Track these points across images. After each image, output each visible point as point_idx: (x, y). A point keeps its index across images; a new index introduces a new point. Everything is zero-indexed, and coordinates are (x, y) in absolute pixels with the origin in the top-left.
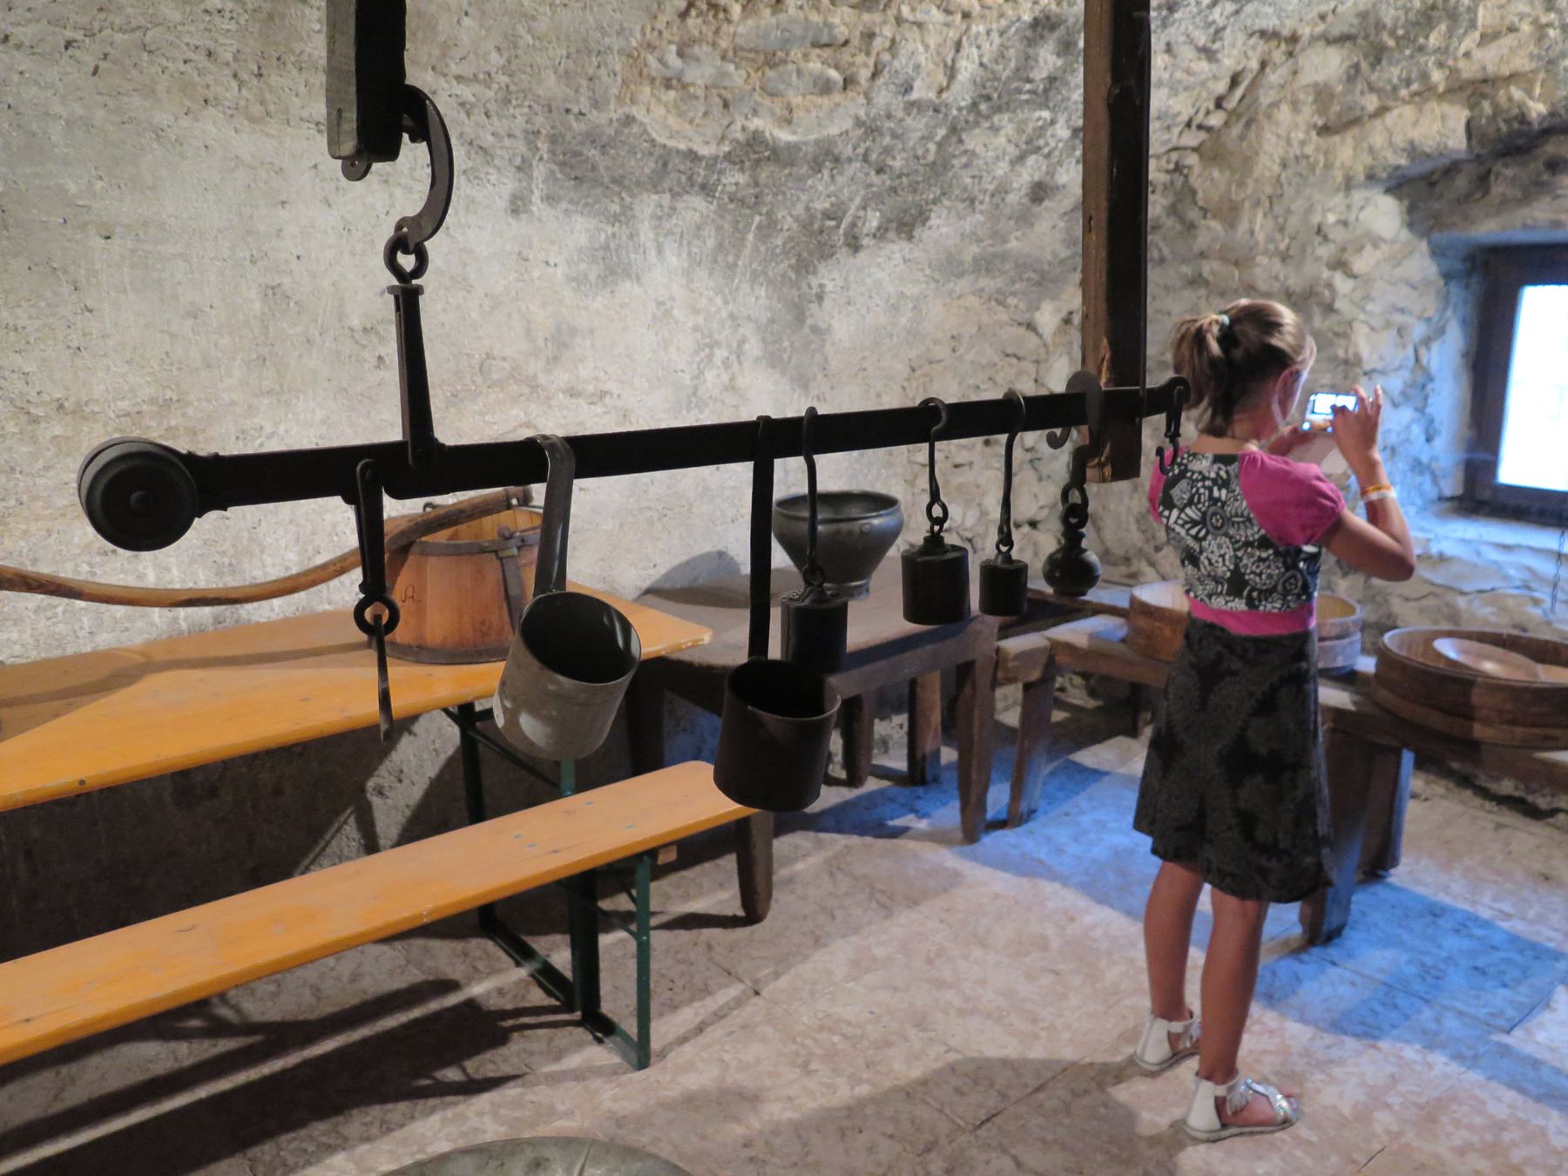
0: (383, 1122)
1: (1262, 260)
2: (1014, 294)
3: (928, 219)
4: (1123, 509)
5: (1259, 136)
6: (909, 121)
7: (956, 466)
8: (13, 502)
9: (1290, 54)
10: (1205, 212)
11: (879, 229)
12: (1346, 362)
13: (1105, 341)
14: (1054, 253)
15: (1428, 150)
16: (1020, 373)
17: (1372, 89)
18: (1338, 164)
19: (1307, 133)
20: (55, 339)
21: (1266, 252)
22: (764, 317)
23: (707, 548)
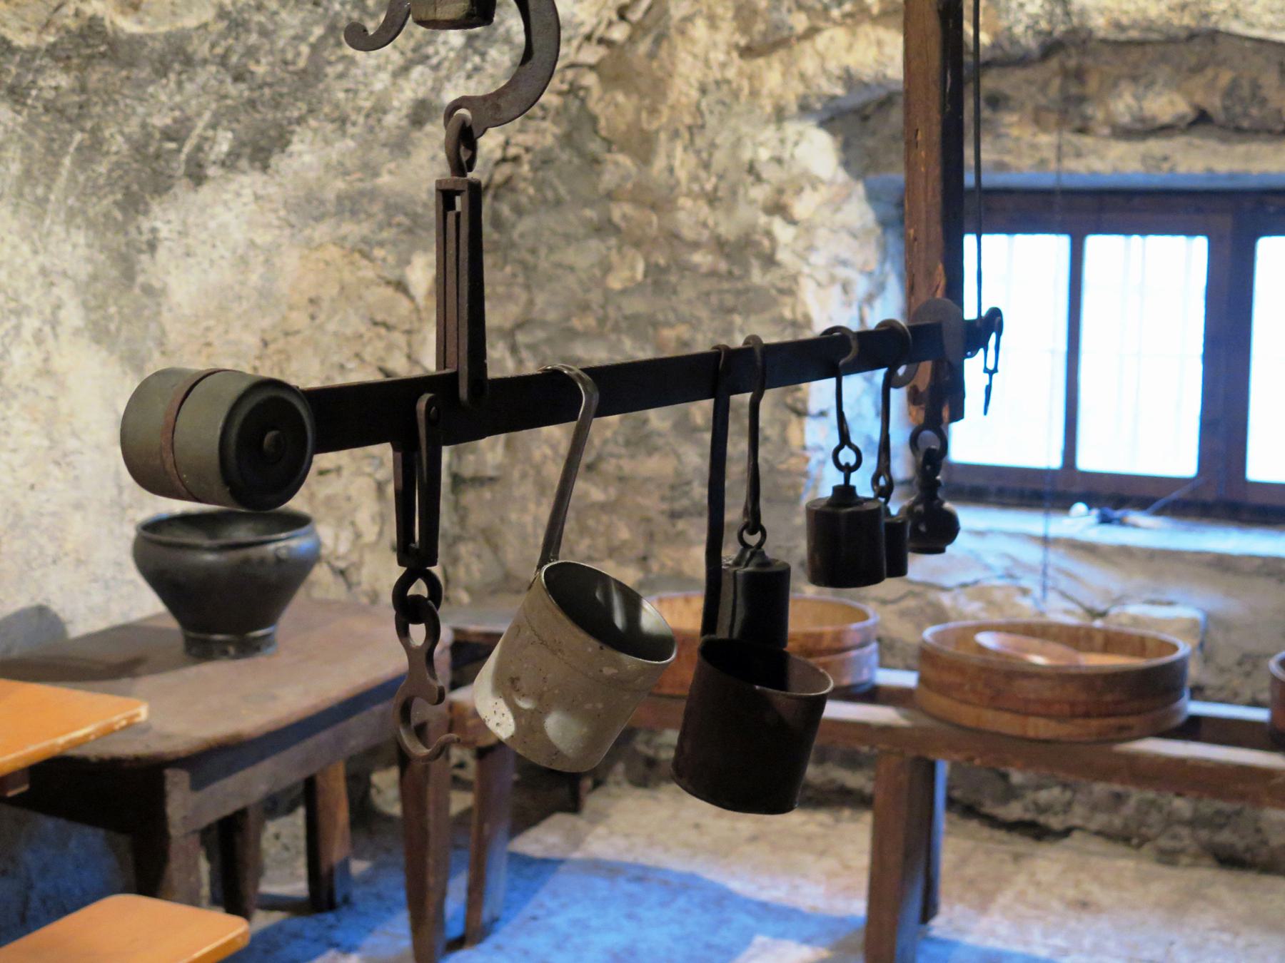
1: (685, 202)
2: (381, 244)
3: (288, 143)
4: (528, 519)
5: (672, 55)
6: (284, 15)
10: (609, 143)
11: (229, 154)
13: (940, 267)
15: (866, 79)
16: (390, 347)
18: (765, 91)
19: (728, 53)
21: (689, 194)
22: (84, 271)
23: (22, 601)
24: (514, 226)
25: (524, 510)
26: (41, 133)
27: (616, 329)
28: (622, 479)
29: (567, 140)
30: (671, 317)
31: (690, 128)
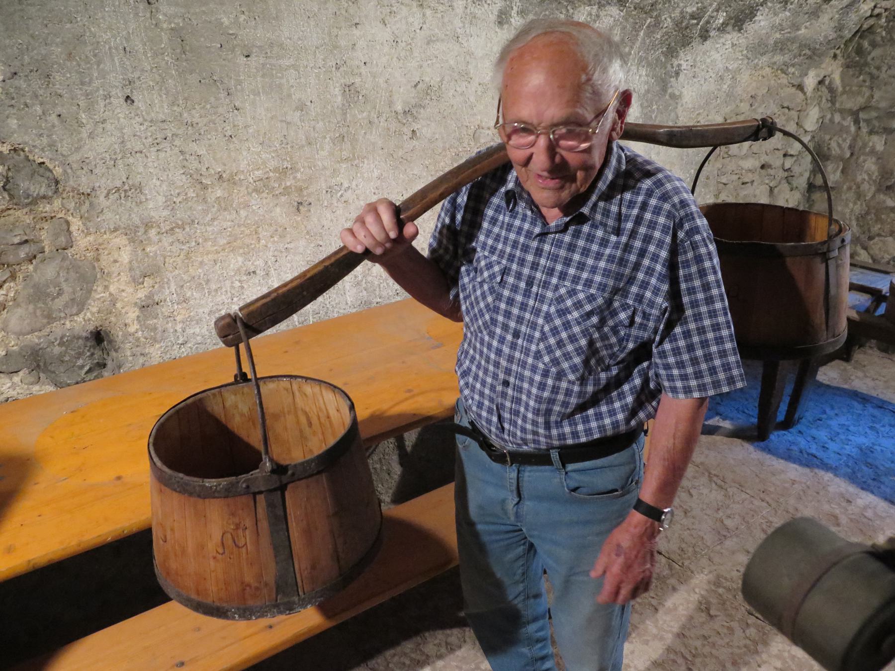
0: (447, 644)
2: (793, 65)
7: (743, 184)
8: (193, 244)
11: (723, 24)
14: (826, 37)
20: (216, 131)
24: (869, 53)
25: (847, 205)
26: (631, 20)
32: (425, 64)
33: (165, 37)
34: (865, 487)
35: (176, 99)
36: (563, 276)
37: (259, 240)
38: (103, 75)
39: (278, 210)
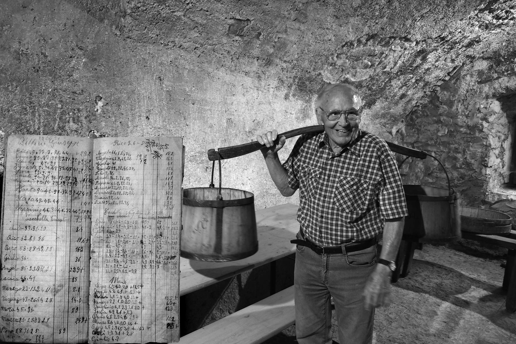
2: (388, 124)
9: (471, 62)
12: (486, 146)
14: (400, 113)
17: (496, 72)
18: (484, 92)
27: (439, 144)
28: (437, 178)
29: (431, 102)
30: (454, 142)
31: (463, 100)
32: (258, 113)
33: (164, 94)
34: (444, 299)
35: (165, 119)
36: (341, 173)
37: (190, 182)
38: (140, 107)
39: (198, 170)
